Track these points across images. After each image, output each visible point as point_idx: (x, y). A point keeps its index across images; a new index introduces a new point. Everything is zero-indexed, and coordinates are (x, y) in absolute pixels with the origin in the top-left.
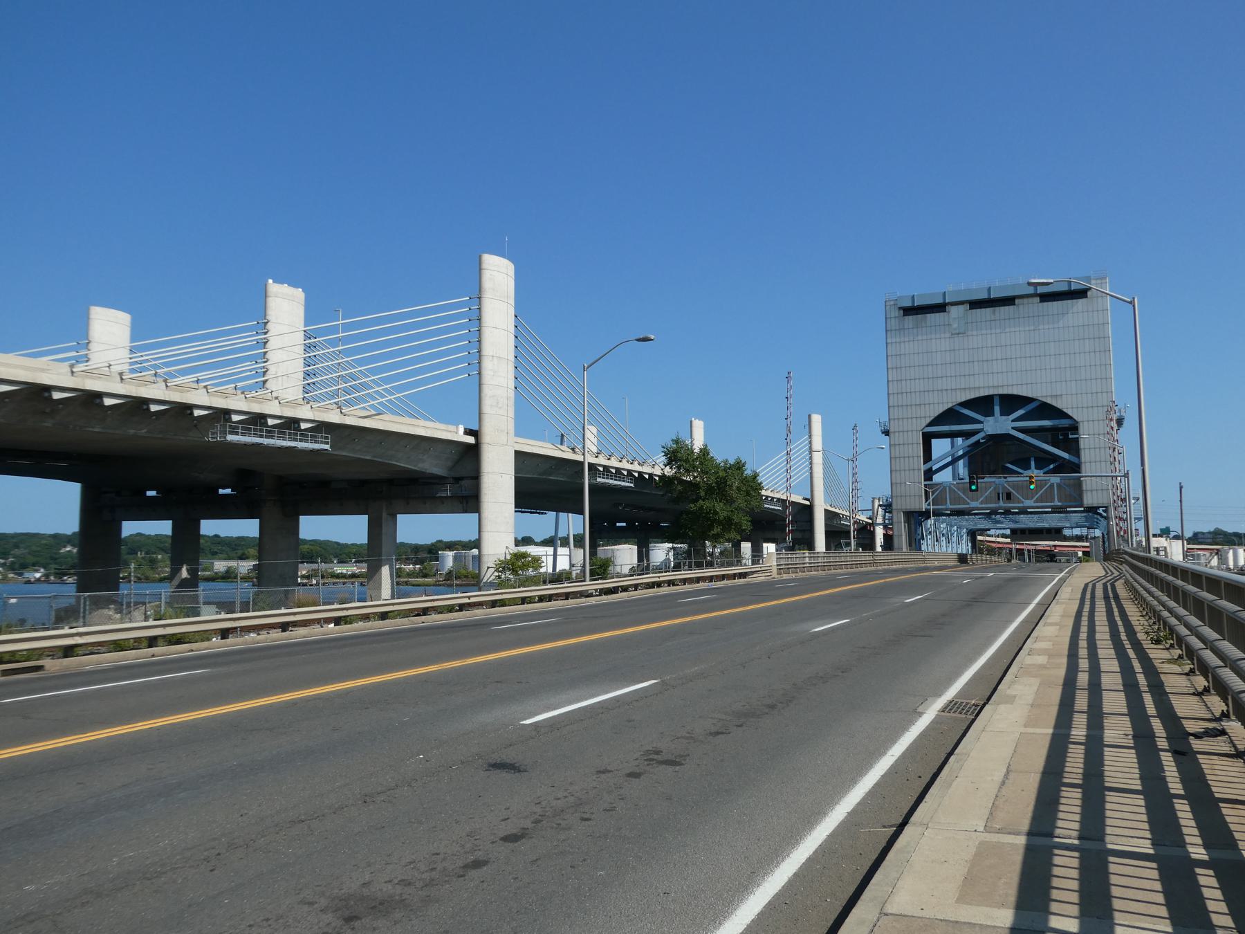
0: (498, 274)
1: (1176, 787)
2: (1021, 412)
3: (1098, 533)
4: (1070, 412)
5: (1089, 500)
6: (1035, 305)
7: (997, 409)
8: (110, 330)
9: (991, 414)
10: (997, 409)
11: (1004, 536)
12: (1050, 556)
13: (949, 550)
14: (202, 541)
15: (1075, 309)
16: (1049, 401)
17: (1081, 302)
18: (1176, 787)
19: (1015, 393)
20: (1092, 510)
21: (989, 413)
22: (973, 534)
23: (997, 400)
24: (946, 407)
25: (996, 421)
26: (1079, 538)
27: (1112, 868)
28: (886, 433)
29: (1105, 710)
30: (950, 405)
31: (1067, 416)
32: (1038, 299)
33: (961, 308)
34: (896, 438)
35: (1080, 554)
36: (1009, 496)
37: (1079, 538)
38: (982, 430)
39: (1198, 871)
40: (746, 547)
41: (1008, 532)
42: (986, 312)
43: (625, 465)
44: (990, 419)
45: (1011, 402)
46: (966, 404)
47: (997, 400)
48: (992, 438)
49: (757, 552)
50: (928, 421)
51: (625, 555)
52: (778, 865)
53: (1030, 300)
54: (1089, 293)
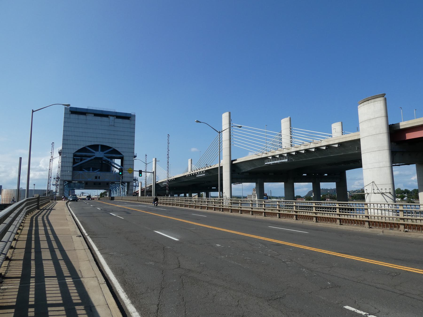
0: (285, 123)
1: (33, 274)
14: (321, 191)
17: (126, 121)
18: (33, 274)
23: (100, 147)
27: (61, 298)
29: (42, 247)
30: (84, 146)
32: (115, 117)
33: (113, 117)
39: (80, 301)
40: (187, 195)
43: (201, 170)
46: (90, 146)
47: (100, 147)
48: (97, 158)
49: (191, 196)
50: (76, 150)
52: (121, 286)
53: (91, 115)
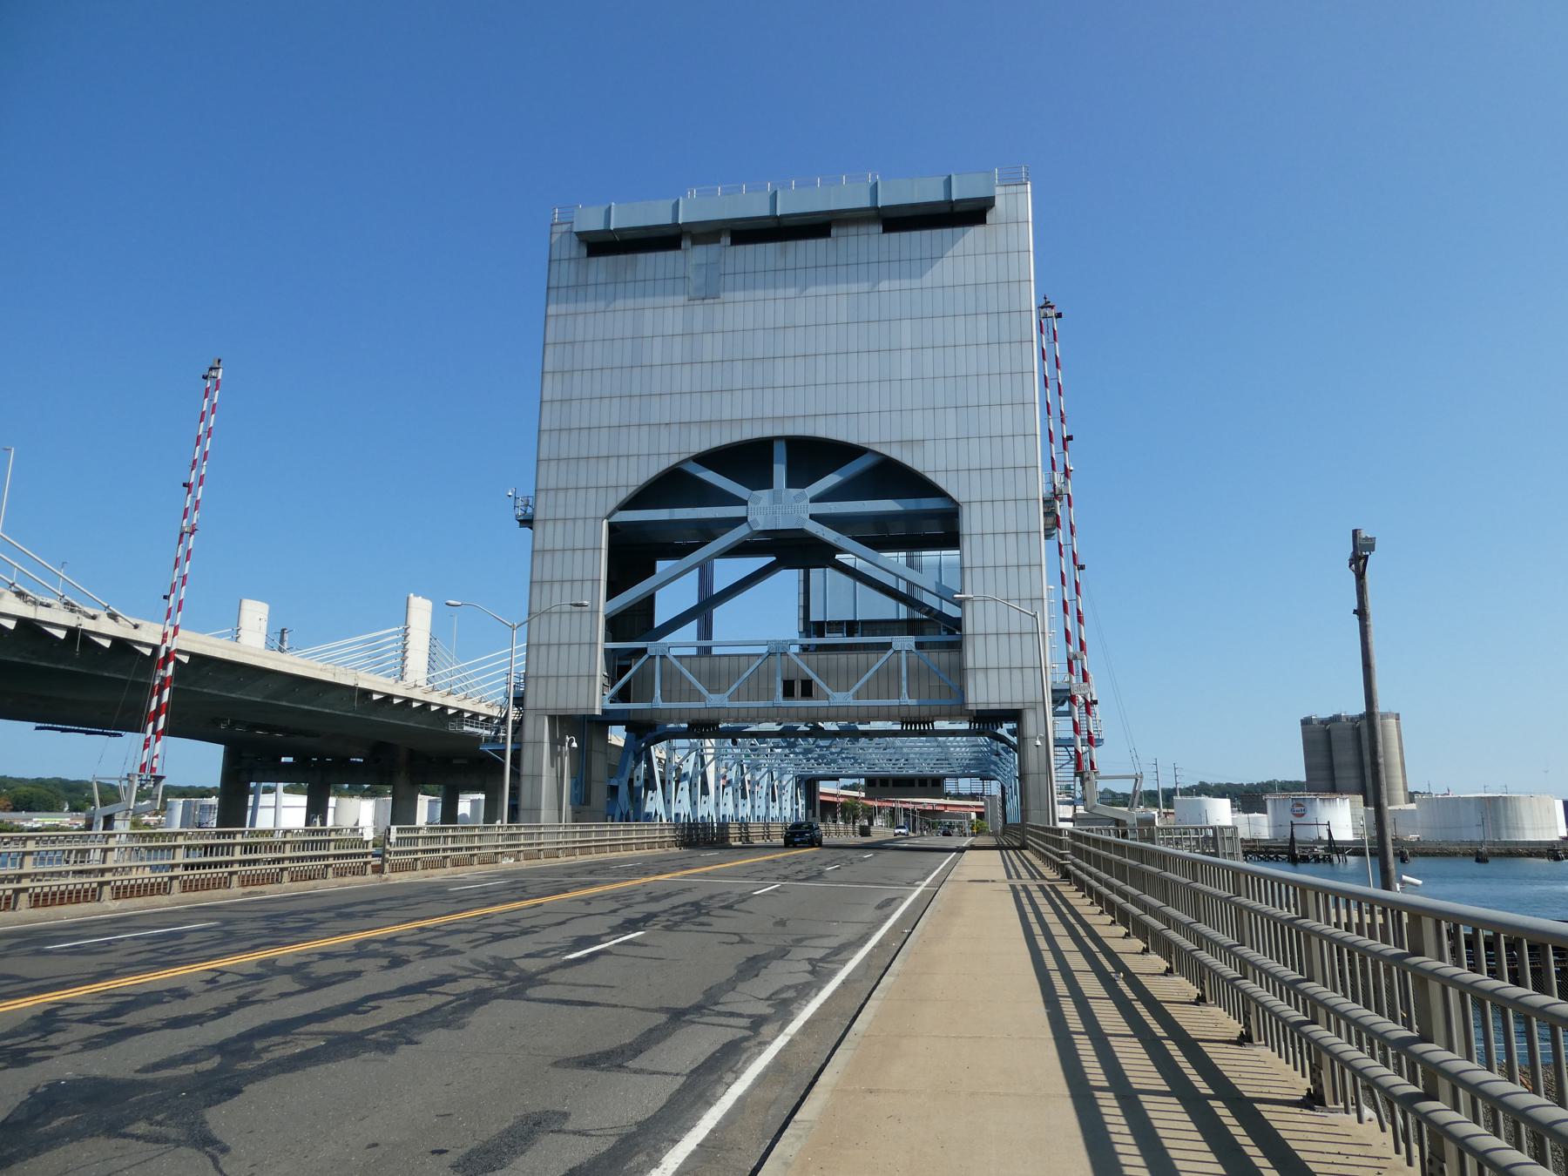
2: (831, 480)
3: (994, 788)
4: (940, 481)
5: (983, 693)
6: (873, 240)
7: (780, 472)
8: (255, 616)
9: (766, 482)
10: (780, 472)
11: (853, 788)
12: (930, 819)
13: (774, 812)
15: (958, 248)
16: (895, 453)
17: (973, 233)
19: (821, 432)
20: (987, 720)
21: (763, 481)
22: (808, 785)
23: (780, 451)
24: (664, 464)
25: (776, 500)
26: (973, 797)
28: (527, 522)
30: (674, 460)
31: (931, 490)
34: (549, 535)
35: (974, 816)
36: (808, 689)
37: (973, 797)
38: (744, 520)
41: (863, 781)
42: (768, 252)
44: (764, 494)
45: (813, 457)
47: (780, 451)
50: (623, 495)
51: (281, 810)
54: (990, 217)
